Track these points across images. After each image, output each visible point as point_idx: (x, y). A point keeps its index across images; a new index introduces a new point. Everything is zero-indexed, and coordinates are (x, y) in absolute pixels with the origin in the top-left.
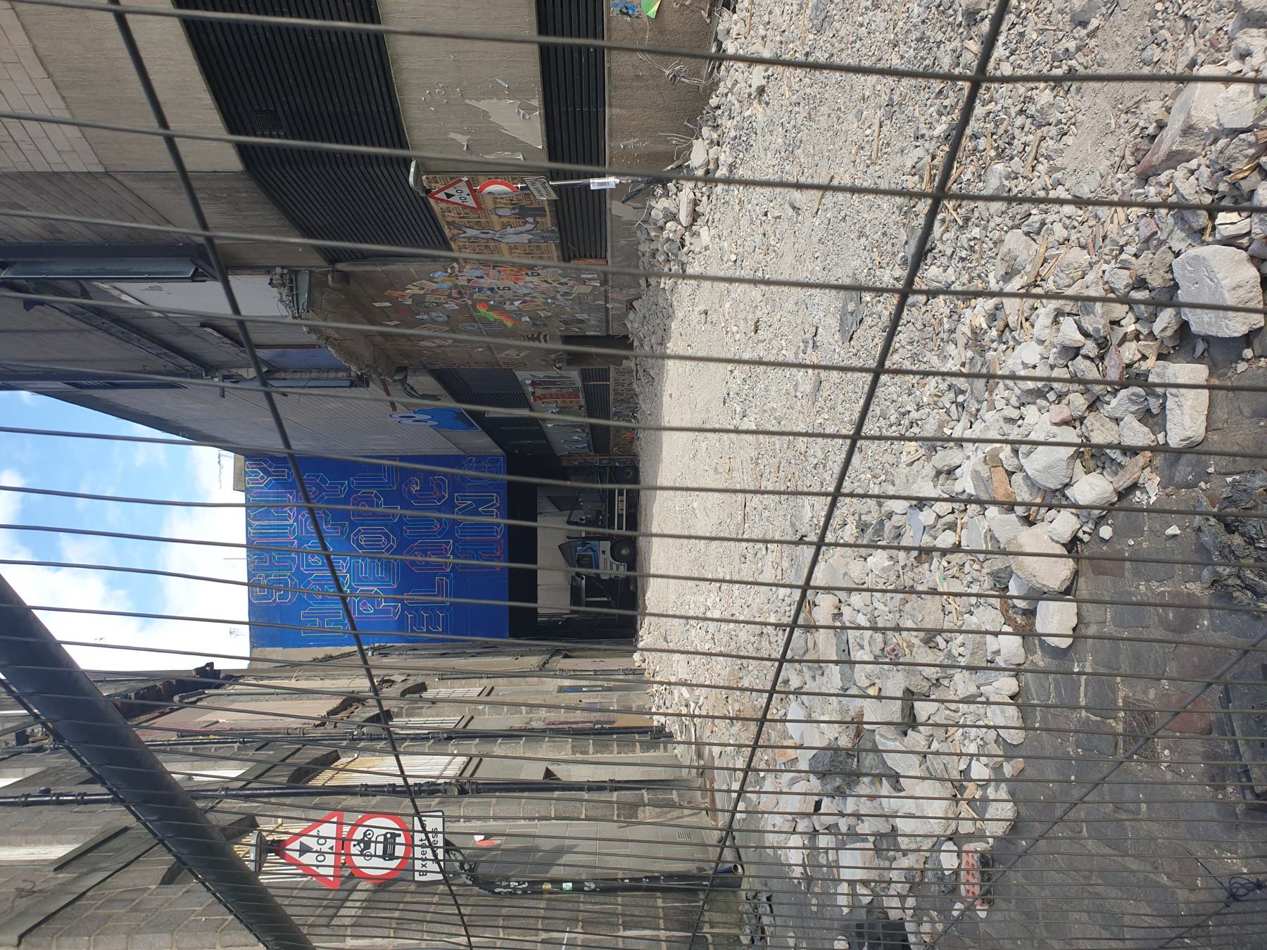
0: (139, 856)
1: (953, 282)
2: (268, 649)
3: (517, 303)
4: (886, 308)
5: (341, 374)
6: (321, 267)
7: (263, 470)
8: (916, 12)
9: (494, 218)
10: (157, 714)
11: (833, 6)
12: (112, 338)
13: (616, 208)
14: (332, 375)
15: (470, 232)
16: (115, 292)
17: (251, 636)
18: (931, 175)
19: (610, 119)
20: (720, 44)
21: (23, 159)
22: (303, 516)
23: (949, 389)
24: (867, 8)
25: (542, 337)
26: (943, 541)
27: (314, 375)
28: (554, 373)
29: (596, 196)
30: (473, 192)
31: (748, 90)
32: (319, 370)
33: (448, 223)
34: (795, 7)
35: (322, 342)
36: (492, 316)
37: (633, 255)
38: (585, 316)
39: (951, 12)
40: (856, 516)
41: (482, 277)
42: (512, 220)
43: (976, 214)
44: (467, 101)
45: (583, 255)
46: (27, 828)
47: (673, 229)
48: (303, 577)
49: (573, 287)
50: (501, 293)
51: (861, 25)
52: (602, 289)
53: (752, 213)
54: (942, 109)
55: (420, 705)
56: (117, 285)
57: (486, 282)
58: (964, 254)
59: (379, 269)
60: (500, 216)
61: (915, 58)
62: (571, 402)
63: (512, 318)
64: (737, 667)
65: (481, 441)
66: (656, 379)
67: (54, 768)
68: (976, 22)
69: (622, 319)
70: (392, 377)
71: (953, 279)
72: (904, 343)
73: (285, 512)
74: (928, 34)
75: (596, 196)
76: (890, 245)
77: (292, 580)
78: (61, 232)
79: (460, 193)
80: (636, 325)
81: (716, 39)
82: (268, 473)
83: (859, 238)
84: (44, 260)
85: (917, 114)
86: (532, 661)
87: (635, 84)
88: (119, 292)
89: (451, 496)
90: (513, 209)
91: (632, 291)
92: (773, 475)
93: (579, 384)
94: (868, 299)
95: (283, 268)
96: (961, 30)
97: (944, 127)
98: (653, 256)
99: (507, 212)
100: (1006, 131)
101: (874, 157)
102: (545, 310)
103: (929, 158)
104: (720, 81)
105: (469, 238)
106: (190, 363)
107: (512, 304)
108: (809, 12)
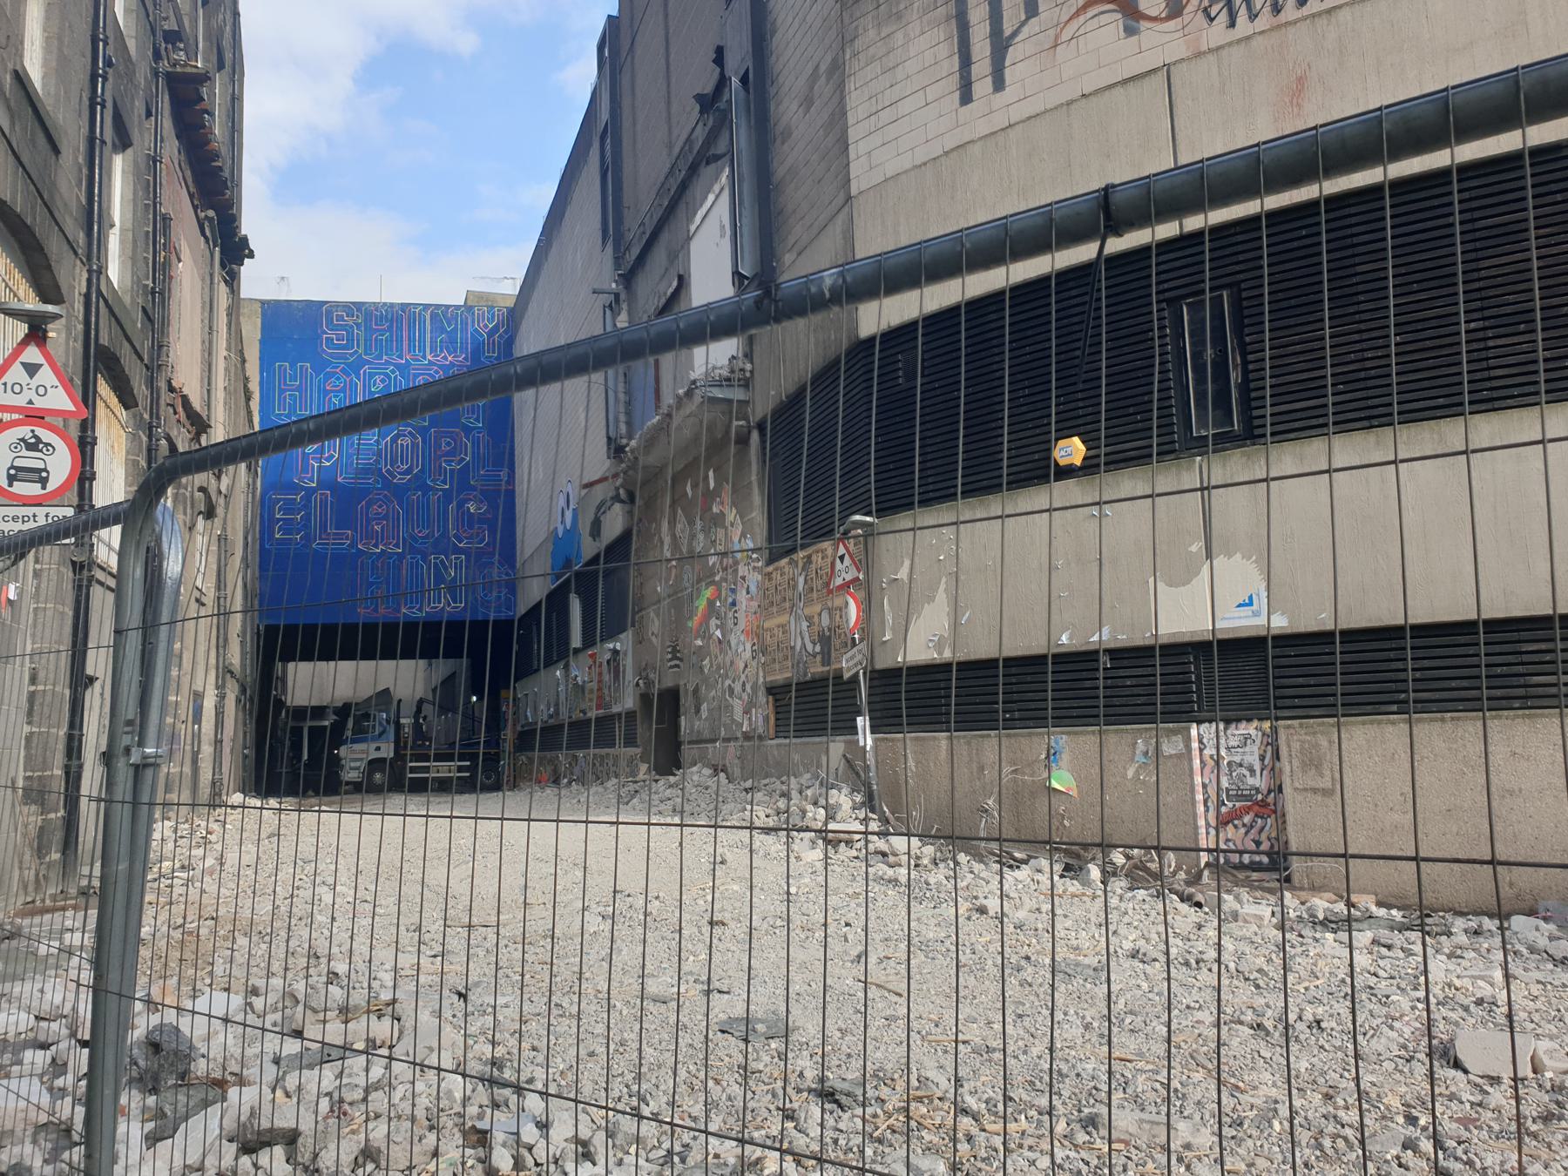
0: (24, 168)
1: (807, 1135)
2: (259, 321)
3: (718, 633)
4: (766, 1065)
5: (623, 428)
6: (753, 411)
7: (496, 329)
8: (1088, 1066)
9: (817, 608)
10: (191, 189)
11: (1081, 982)
12: (662, 178)
13: (837, 747)
14: (622, 418)
15: (801, 580)
16: (717, 188)
17: (278, 302)
18: (921, 1098)
19: (935, 738)
20: (1025, 862)
21: (860, 118)
22: (437, 372)
23: (683, 1146)
24: (1083, 1018)
25: (677, 662)
26: (502, 1157)
27: (622, 396)
28: (630, 676)
29: (849, 724)
30: (846, 585)
31: (981, 895)
32: (628, 403)
33: (809, 557)
34: (1075, 943)
35: (664, 410)
36: (702, 604)
37: (785, 770)
38: (704, 714)
39: (1092, 1101)
40: (507, 1056)
41: (748, 593)
42: (816, 628)
43: (887, 1150)
44: (944, 580)
45: (779, 710)
46: (66, 40)
47: (818, 817)
48: (356, 367)
49: (740, 698)
50: (730, 615)
51: (1065, 1014)
52: (739, 735)
53: (847, 909)
54: (993, 1102)
55: (189, 511)
56: (726, 193)
57: (742, 596)
58: (842, 1142)
59: (754, 478)
60: (820, 615)
61: (1041, 1071)
62: (591, 700)
63: (701, 624)
64: (261, 928)
65: (534, 591)
66: (628, 807)
67: (134, 72)
68: (1084, 1127)
69: (702, 759)
70: (622, 486)
71: (812, 1135)
72: (728, 1091)
73: (442, 351)
74: (1067, 1080)
75: (849, 724)
76: (838, 1063)
77: (352, 355)
78: (783, 143)
79: (846, 571)
80: (695, 778)
81: (1030, 857)
82: (491, 333)
83: (840, 1030)
84: (753, 122)
85: (983, 1078)
86: (235, 657)
87: (975, 765)
88: (717, 192)
89: (458, 551)
90: (830, 630)
91: (737, 772)
92: (534, 957)
93: (616, 709)
94: (773, 1045)
95: (752, 372)
96: (1076, 1113)
97: (975, 1107)
98: (783, 795)
99: (825, 621)
100: (980, 1170)
101: (930, 1037)
102: (711, 666)
103: (940, 1094)
104: (986, 864)
105: (793, 579)
106: (633, 258)
107: (717, 627)
108: (1072, 956)
